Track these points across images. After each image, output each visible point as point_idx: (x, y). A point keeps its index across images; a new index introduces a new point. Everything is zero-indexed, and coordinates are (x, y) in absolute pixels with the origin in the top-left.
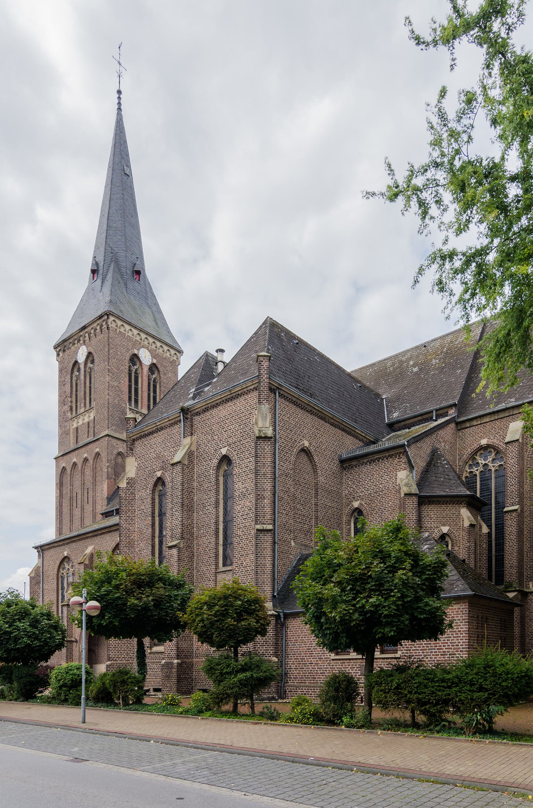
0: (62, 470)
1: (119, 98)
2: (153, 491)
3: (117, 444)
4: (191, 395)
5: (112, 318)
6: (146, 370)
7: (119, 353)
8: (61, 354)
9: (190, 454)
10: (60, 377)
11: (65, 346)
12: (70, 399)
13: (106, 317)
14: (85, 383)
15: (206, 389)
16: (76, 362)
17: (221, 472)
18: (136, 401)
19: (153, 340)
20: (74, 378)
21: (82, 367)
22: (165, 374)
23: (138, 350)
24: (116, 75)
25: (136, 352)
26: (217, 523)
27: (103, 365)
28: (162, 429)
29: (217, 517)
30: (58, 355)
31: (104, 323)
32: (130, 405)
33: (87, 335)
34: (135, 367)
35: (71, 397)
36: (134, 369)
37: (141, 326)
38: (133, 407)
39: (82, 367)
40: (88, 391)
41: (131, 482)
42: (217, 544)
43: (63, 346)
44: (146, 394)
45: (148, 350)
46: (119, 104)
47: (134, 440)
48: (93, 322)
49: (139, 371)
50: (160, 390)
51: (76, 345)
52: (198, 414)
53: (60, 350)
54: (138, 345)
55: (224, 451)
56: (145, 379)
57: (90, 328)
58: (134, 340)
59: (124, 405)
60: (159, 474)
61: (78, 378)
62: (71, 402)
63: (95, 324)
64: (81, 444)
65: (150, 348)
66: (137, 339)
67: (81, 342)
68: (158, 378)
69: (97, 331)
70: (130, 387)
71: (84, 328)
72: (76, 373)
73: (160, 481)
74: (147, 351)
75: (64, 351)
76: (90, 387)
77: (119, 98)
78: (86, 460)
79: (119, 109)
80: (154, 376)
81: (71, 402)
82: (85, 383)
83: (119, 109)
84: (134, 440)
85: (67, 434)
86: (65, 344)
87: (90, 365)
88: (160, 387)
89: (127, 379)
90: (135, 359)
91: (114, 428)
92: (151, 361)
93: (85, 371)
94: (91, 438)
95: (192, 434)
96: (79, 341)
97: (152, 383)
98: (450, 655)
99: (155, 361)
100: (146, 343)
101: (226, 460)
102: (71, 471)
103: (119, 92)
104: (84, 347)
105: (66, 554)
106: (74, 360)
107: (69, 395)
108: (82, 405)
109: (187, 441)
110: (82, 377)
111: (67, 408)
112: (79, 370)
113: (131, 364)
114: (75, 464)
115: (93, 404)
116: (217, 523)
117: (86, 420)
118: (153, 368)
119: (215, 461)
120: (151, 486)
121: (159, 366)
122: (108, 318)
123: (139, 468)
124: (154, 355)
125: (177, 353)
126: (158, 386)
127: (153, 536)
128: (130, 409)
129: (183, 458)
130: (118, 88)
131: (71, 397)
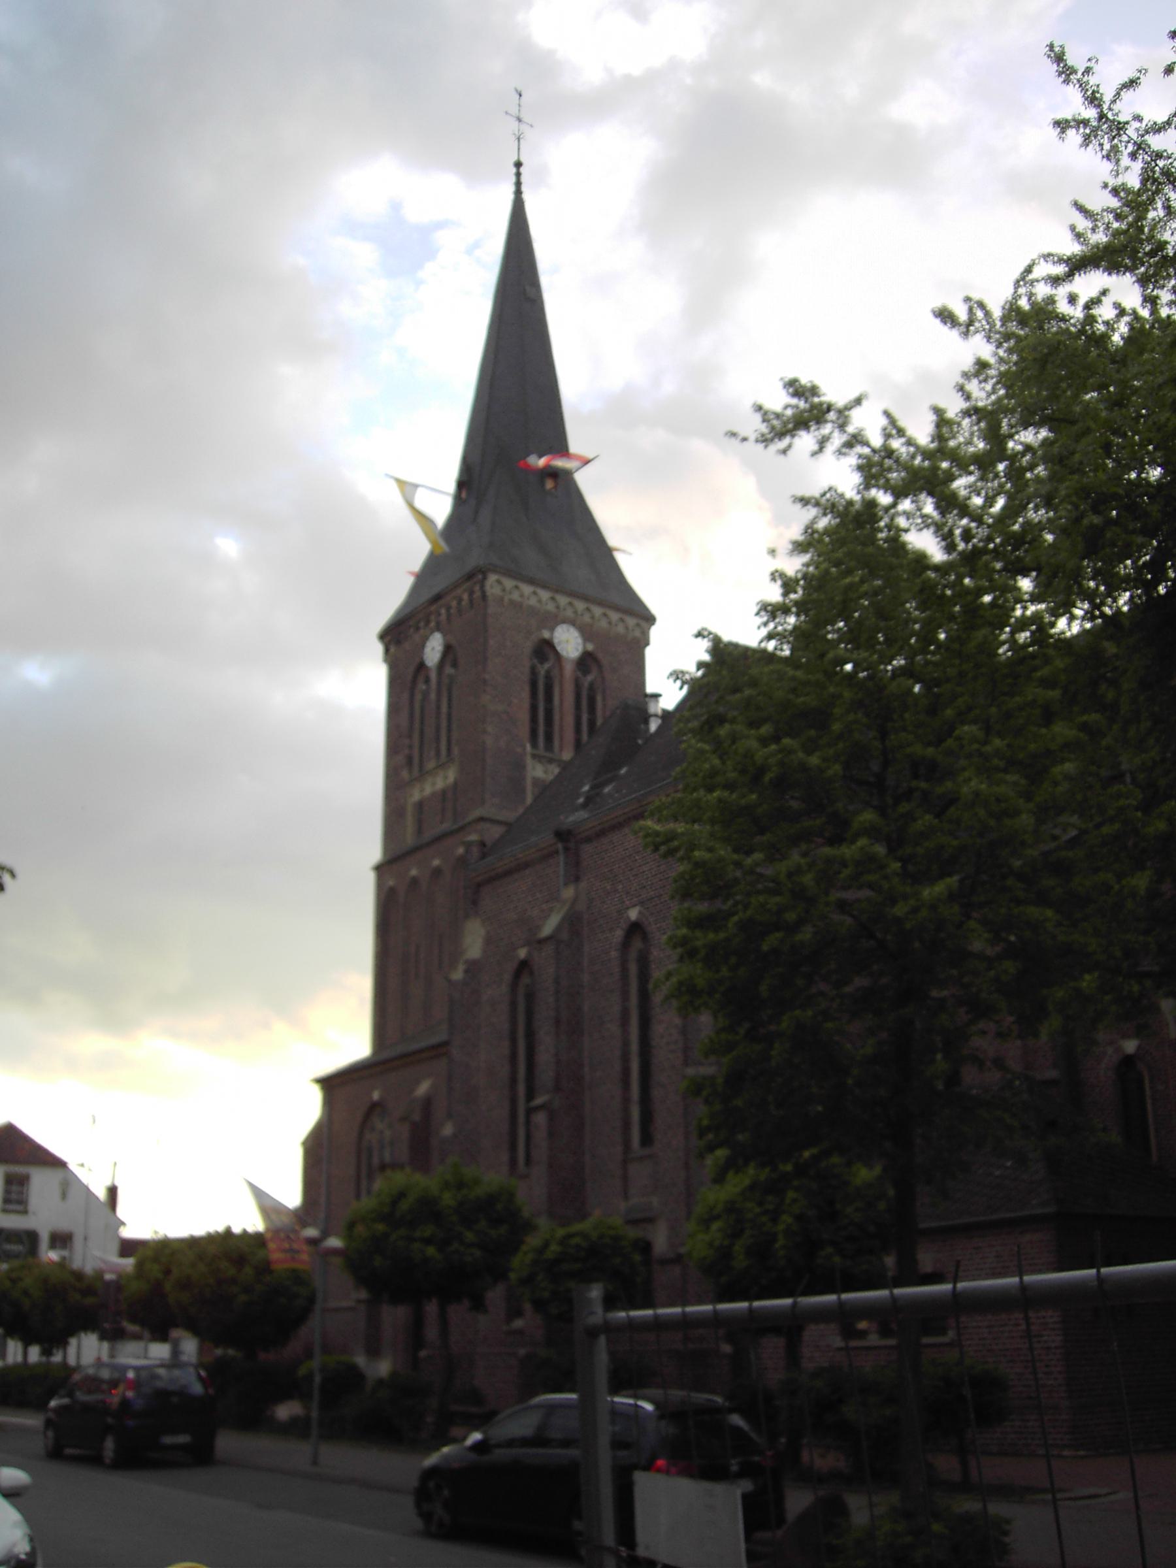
1: (518, 175)
2: (514, 986)
4: (581, 800)
5: (492, 578)
9: (573, 921)
13: (480, 576)
14: (438, 707)
15: (607, 790)
16: (422, 666)
17: (633, 954)
18: (549, 738)
20: (418, 697)
21: (433, 676)
23: (552, 629)
24: (514, 138)
25: (546, 634)
26: (625, 1058)
28: (527, 865)
29: (626, 1044)
31: (477, 588)
32: (534, 745)
33: (443, 611)
34: (547, 666)
36: (542, 670)
38: (541, 749)
39: (433, 676)
40: (444, 724)
41: (473, 968)
42: (626, 1100)
44: (569, 720)
47: (479, 885)
48: (456, 585)
52: (589, 840)
54: (554, 620)
55: (633, 914)
56: (569, 688)
59: (519, 750)
60: (522, 953)
61: (425, 695)
63: (459, 591)
64: (428, 835)
67: (433, 624)
69: (463, 603)
70: (534, 709)
71: (437, 598)
72: (422, 686)
73: (524, 966)
76: (449, 715)
77: (518, 175)
78: (437, 873)
80: (590, 678)
81: (411, 747)
84: (479, 885)
87: (449, 670)
88: (604, 699)
89: (526, 694)
90: (545, 650)
93: (439, 683)
94: (446, 826)
95: (577, 879)
96: (428, 622)
97: (584, 693)
99: (590, 647)
100: (569, 613)
101: (635, 929)
103: (518, 165)
105: (376, 1096)
108: (433, 753)
109: (568, 893)
110: (433, 696)
112: (427, 680)
113: (535, 661)
114: (415, 881)
115: (456, 751)
116: (625, 1058)
118: (586, 661)
119: (619, 934)
120: (508, 977)
121: (600, 656)
122: (485, 578)
123: (489, 941)
124: (587, 633)
126: (599, 698)
127: (513, 1081)
129: (558, 929)
131: (410, 737)
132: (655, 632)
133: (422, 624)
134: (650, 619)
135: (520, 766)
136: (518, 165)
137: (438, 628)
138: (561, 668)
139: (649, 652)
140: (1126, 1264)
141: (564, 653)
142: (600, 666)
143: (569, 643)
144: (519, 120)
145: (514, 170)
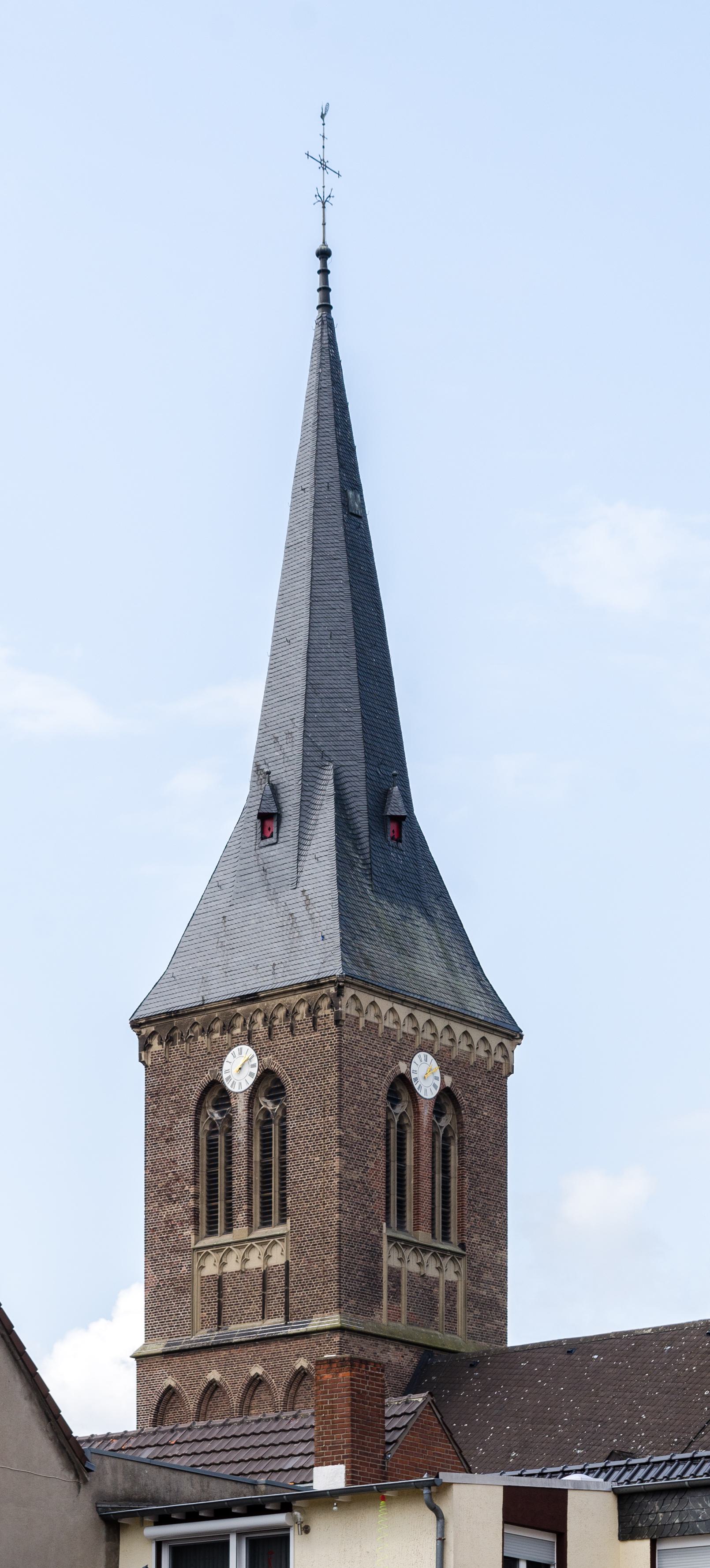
0: (164, 1394)
1: (324, 272)
3: (362, 1350)
6: (426, 1112)
7: (364, 1084)
8: (156, 1046)
10: (150, 1113)
11: (174, 1028)
12: (192, 1190)
14: (250, 1154)
19: (446, 1023)
21: (240, 1106)
22: (474, 1112)
23: (409, 1061)
25: (403, 1067)
27: (319, 1121)
30: (145, 1046)
35: (196, 1183)
37: (416, 991)
39: (240, 1106)
43: (160, 1029)
45: (431, 1053)
46: (325, 290)
49: (410, 1119)
50: (462, 1163)
51: (217, 1036)
53: (154, 1033)
54: (407, 1048)
57: (272, 1003)
58: (400, 1036)
59: (374, 1232)
62: (196, 1197)
63: (293, 999)
65: (436, 1049)
66: (405, 1030)
68: (454, 1127)
71: (253, 998)
74: (430, 1057)
75: (170, 1040)
77: (324, 272)
79: (325, 306)
82: (250, 1154)
83: (325, 306)
85: (184, 1291)
86: (176, 1022)
88: (461, 1152)
91: (352, 1302)
92: (438, 1083)
93: (250, 1120)
96: (227, 1028)
98: (326, 1387)
99: (448, 1081)
102: (200, 1404)
103: (324, 254)
104: (247, 1051)
106: (207, 1077)
107: (190, 1175)
111: (178, 1210)
117: (255, 1262)
124: (446, 1066)
125: (505, 1041)
126: (454, 1149)
128: (391, 1239)
130: (318, 245)
132: (520, 1054)
133: (218, 1025)
134: (514, 1035)
135: (376, 1255)
136: (324, 254)
137: (249, 1039)
138: (417, 1113)
139: (510, 1080)
140: (381, 1287)
141: (422, 1093)
142: (457, 1107)
143: (426, 1077)
144: (324, 165)
145: (317, 264)
